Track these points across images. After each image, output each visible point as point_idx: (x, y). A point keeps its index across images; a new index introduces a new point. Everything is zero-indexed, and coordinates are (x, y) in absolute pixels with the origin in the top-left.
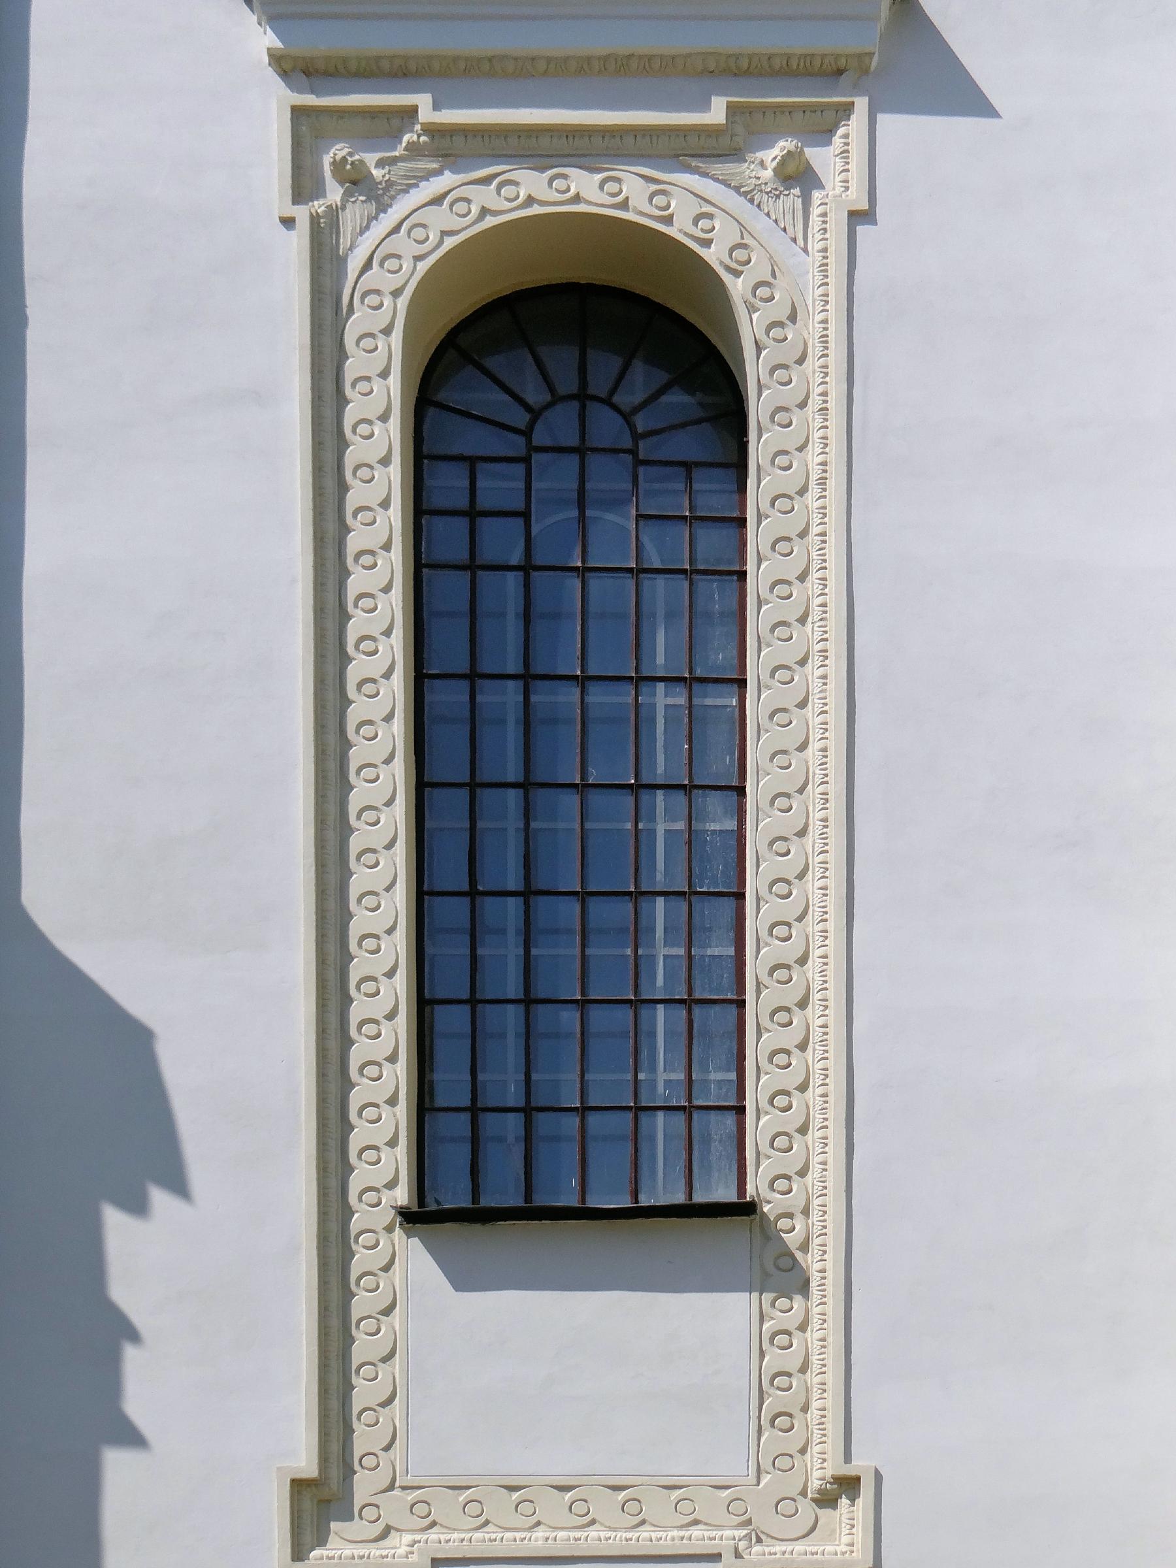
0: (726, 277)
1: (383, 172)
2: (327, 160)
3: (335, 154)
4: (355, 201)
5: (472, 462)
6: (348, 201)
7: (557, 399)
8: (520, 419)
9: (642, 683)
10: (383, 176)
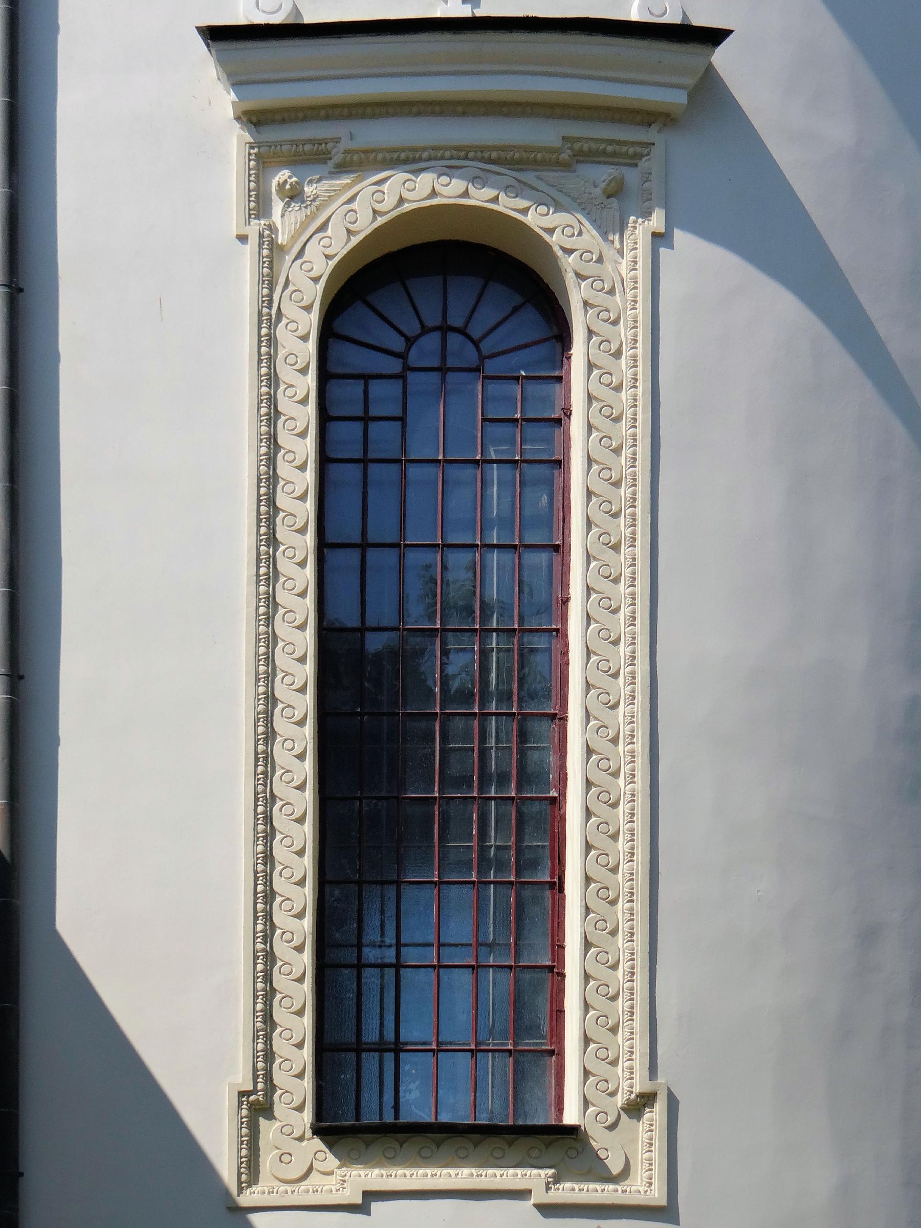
0: (545, 236)
1: (311, 189)
2: (274, 183)
3: (280, 178)
4: (291, 211)
5: (366, 378)
6: (286, 211)
7: (425, 330)
8: (398, 344)
9: (479, 970)
10: (312, 192)
